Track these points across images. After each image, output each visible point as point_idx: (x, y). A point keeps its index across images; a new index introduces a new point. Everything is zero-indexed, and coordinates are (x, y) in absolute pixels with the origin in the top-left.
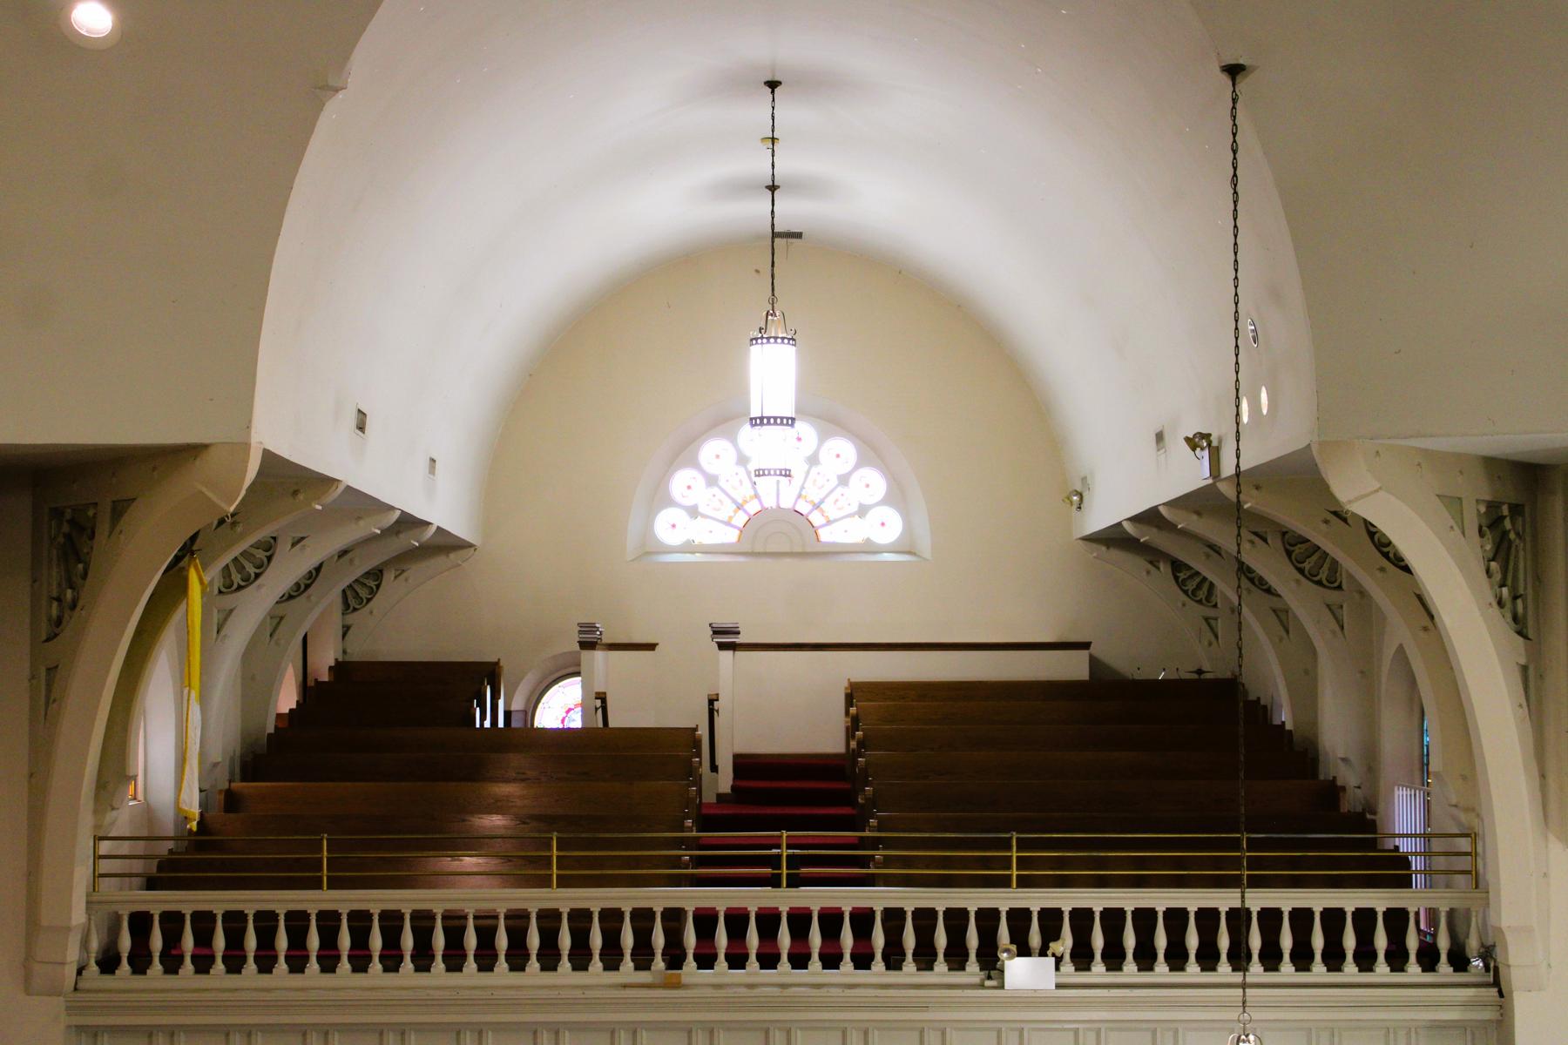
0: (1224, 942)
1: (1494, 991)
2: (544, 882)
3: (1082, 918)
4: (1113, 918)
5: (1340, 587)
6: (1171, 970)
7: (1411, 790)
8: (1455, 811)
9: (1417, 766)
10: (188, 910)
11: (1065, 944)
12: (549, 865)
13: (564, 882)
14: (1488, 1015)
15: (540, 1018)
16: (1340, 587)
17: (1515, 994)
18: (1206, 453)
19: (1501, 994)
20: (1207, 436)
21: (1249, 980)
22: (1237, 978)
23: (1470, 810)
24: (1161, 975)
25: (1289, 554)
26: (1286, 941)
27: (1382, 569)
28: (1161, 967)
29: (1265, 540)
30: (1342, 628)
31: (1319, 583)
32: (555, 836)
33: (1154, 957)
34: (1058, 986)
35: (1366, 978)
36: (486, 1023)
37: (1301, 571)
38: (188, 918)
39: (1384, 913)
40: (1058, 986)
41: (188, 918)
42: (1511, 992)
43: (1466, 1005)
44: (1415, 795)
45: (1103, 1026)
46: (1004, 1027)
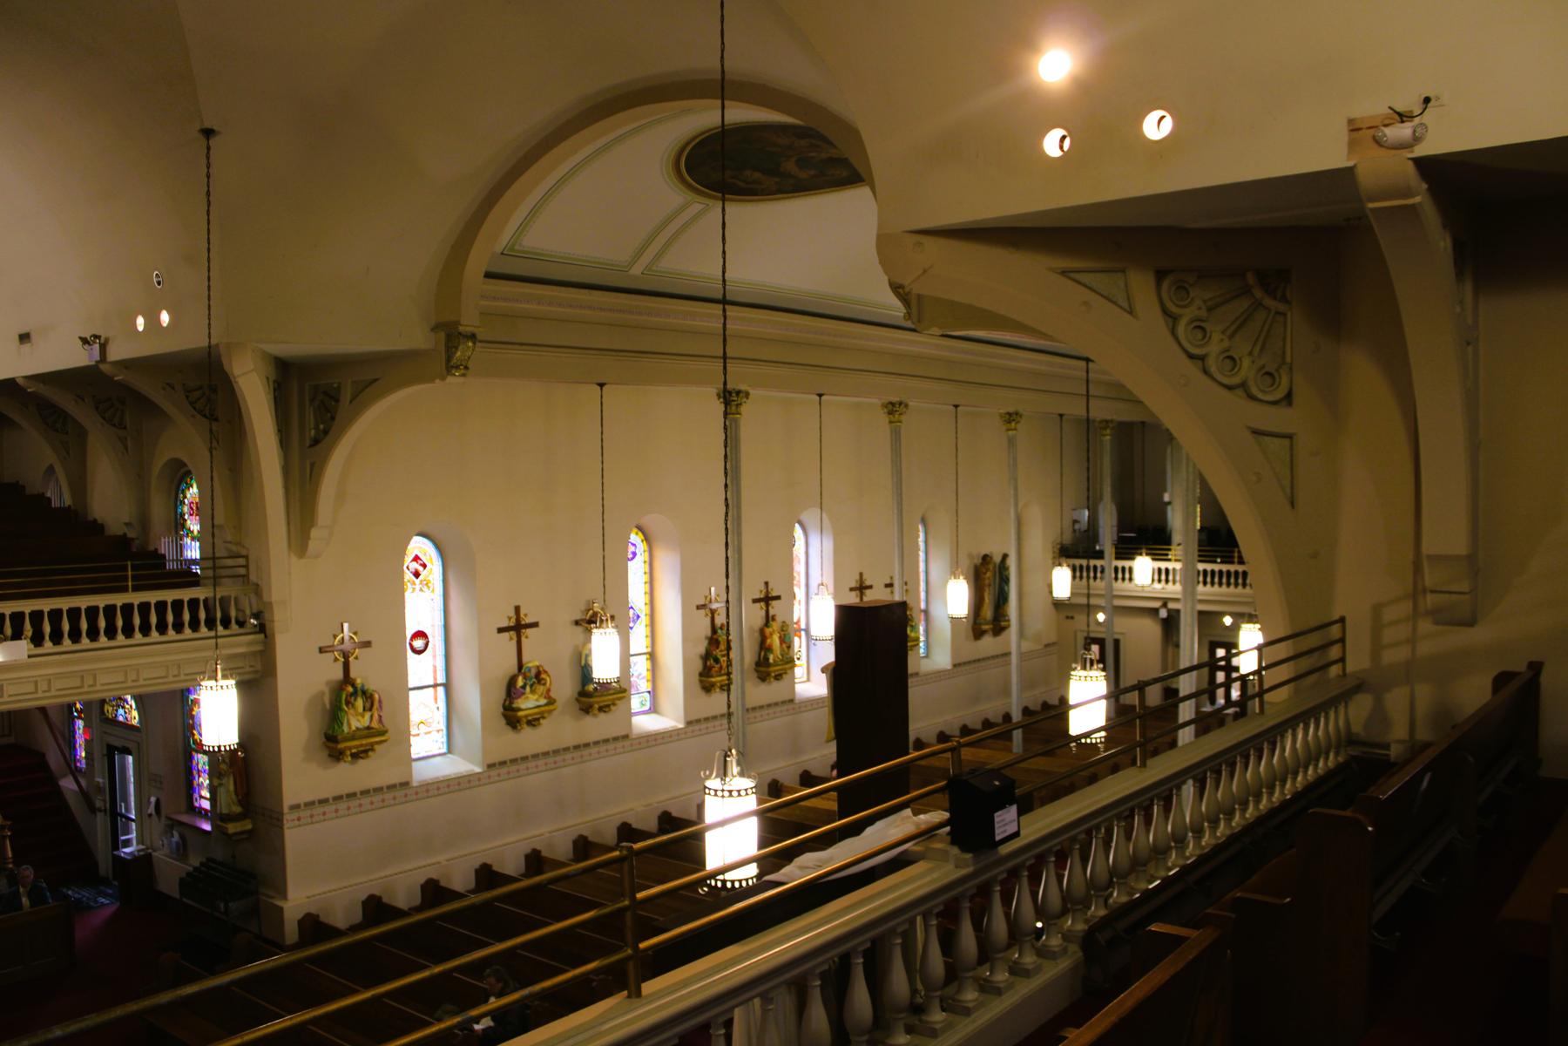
0: (120, 623)
1: (262, 636)
2: (124, 590)
3: (37, 616)
4: (55, 615)
5: (67, 433)
6: (54, 644)
7: (169, 538)
8: (230, 546)
9: (173, 524)
10: (27, 611)
11: (28, 629)
12: (133, 577)
13: (136, 589)
14: (259, 648)
15: (127, 662)
16: (125, 428)
17: (276, 636)
18: (98, 346)
19: (266, 636)
20: (96, 337)
21: (219, 634)
22: (212, 634)
23: (239, 544)
24: (48, 648)
25: (97, 408)
26: (102, 624)
27: (193, 416)
28: (67, 642)
29: (83, 400)
30: (127, 449)
31: (114, 425)
32: (129, 563)
33: (133, 630)
34: (29, 656)
35: (196, 635)
36: (40, 676)
37: (104, 418)
38: (46, 614)
39: (10, 615)
40: (29, 656)
41: (46, 614)
42: (273, 635)
43: (250, 644)
44: (172, 541)
45: (39, 679)
46: (39, 679)
